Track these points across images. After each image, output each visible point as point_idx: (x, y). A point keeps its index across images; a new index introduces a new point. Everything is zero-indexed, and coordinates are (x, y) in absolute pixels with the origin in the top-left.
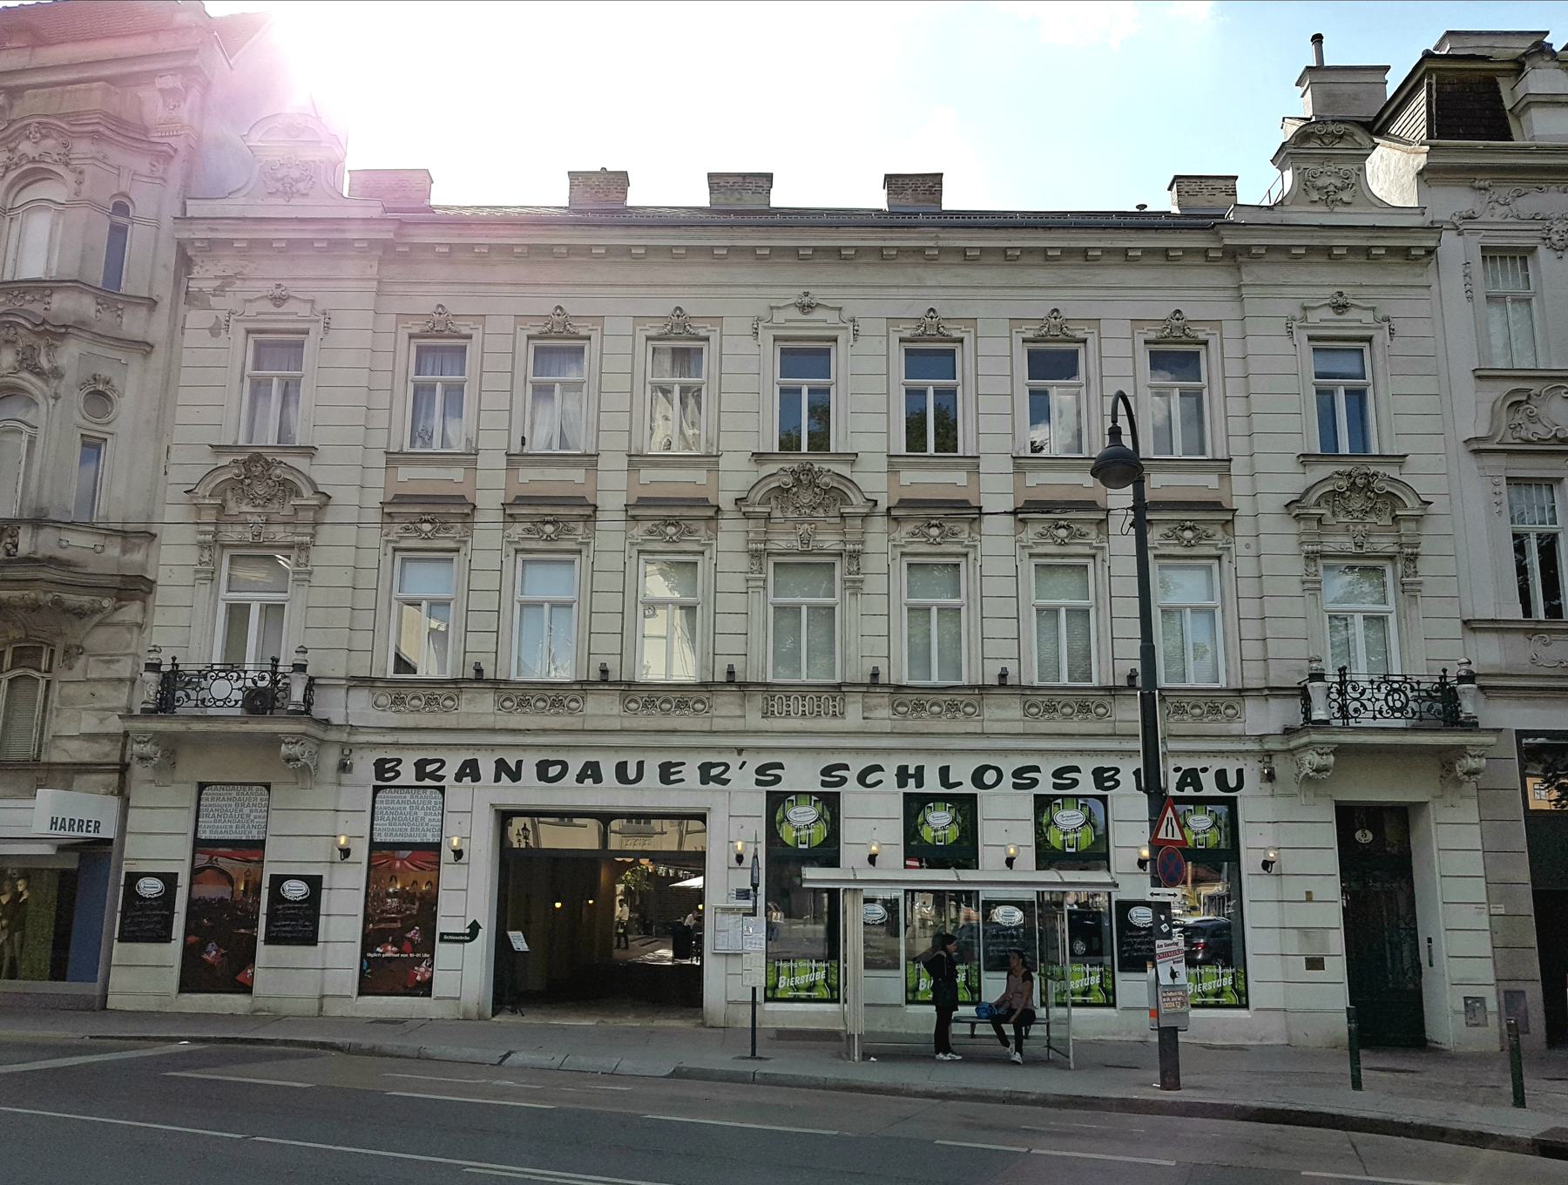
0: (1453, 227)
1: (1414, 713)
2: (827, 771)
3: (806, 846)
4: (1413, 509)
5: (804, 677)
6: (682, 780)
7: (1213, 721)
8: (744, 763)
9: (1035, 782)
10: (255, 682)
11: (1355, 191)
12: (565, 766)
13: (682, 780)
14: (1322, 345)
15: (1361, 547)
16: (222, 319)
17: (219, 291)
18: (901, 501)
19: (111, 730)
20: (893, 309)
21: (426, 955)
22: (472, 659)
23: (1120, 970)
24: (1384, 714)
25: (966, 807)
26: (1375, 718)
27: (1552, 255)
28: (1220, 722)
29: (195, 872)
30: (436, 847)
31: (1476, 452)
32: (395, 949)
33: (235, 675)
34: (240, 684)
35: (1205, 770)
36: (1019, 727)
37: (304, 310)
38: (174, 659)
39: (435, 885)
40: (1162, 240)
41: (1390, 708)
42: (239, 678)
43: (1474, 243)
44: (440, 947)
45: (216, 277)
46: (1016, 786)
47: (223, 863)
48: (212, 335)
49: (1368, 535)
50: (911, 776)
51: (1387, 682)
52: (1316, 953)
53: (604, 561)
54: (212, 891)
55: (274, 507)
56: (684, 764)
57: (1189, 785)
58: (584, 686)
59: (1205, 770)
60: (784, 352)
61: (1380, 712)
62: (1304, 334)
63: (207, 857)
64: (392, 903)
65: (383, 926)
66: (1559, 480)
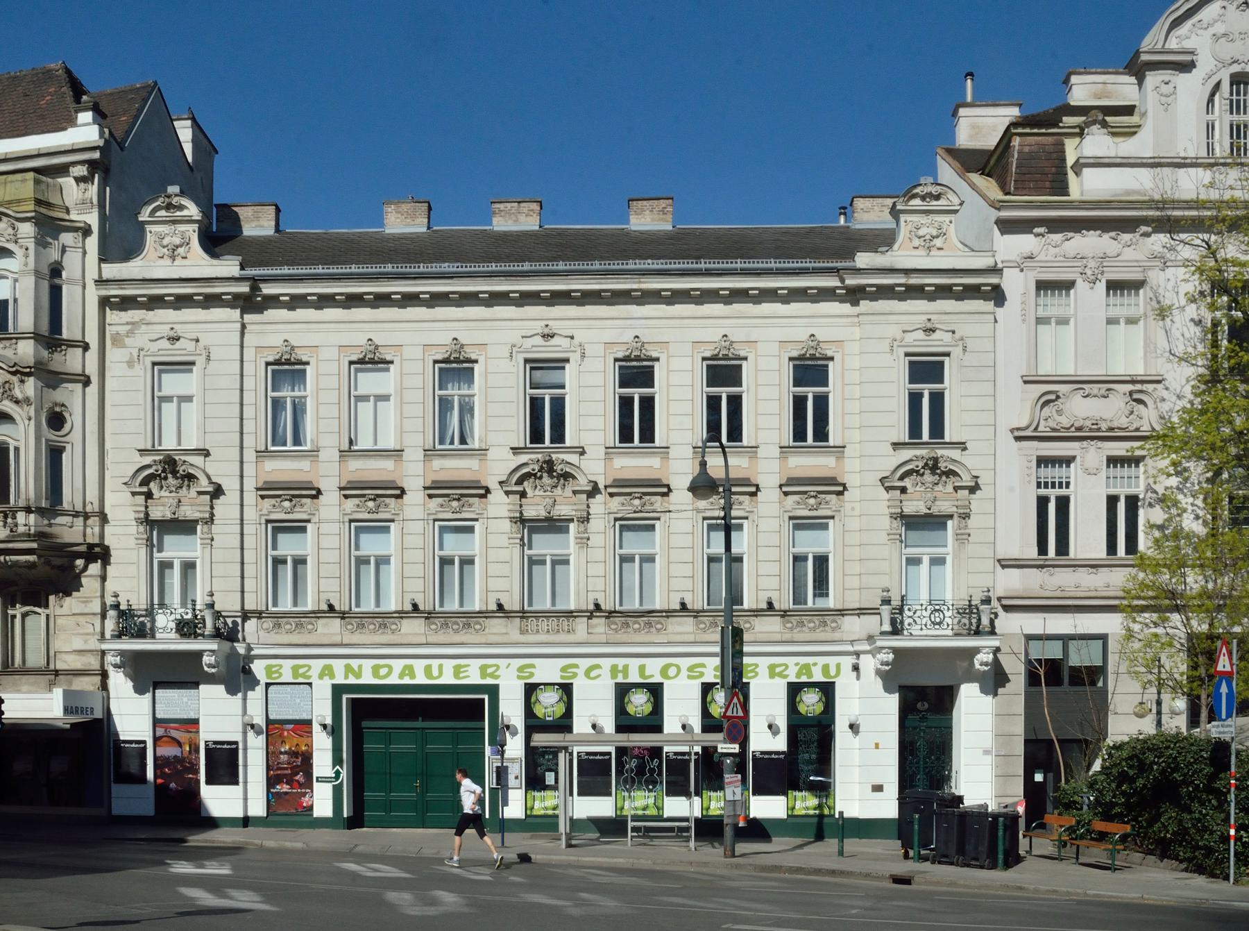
0: (1016, 265)
1: (948, 625)
2: (564, 669)
3: (551, 719)
4: (966, 481)
5: (810, 604)
6: (468, 676)
7: (799, 631)
8: (509, 664)
9: (702, 674)
10: (181, 616)
11: (946, 239)
12: (390, 668)
13: (468, 676)
14: (535, 364)
15: (929, 509)
16: (135, 355)
17: (130, 333)
18: (789, 479)
19: (92, 647)
20: (610, 336)
21: (308, 790)
22: (324, 597)
23: (580, 794)
24: (928, 627)
25: (655, 691)
26: (921, 629)
27: (1087, 285)
28: (827, 631)
29: (156, 740)
30: (308, 723)
31: (1018, 439)
32: (288, 787)
33: (168, 611)
34: (173, 617)
35: (815, 664)
36: (691, 638)
37: (565, 343)
38: (128, 601)
39: (310, 746)
40: (777, 281)
41: (932, 622)
42: (172, 613)
43: (1032, 277)
44: (315, 784)
45: (128, 323)
46: (689, 677)
47: (174, 734)
48: (129, 367)
49: (935, 499)
50: (620, 671)
51: (931, 605)
52: (878, 782)
53: (764, 525)
54: (168, 751)
55: (184, 491)
56: (469, 665)
57: (804, 674)
58: (401, 615)
59: (815, 664)
60: (912, 364)
61: (926, 625)
62: (902, 351)
63: (163, 730)
64: (284, 758)
65: (279, 772)
66: (1074, 458)
